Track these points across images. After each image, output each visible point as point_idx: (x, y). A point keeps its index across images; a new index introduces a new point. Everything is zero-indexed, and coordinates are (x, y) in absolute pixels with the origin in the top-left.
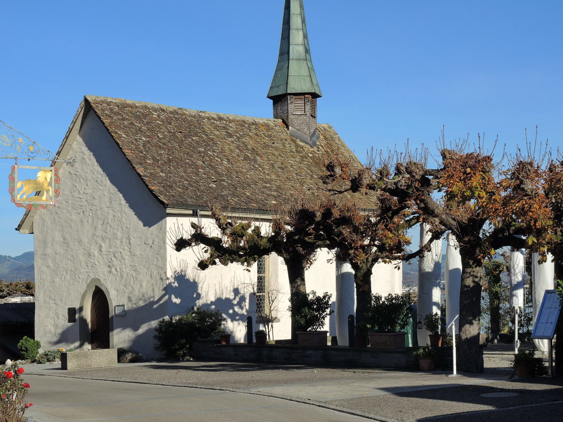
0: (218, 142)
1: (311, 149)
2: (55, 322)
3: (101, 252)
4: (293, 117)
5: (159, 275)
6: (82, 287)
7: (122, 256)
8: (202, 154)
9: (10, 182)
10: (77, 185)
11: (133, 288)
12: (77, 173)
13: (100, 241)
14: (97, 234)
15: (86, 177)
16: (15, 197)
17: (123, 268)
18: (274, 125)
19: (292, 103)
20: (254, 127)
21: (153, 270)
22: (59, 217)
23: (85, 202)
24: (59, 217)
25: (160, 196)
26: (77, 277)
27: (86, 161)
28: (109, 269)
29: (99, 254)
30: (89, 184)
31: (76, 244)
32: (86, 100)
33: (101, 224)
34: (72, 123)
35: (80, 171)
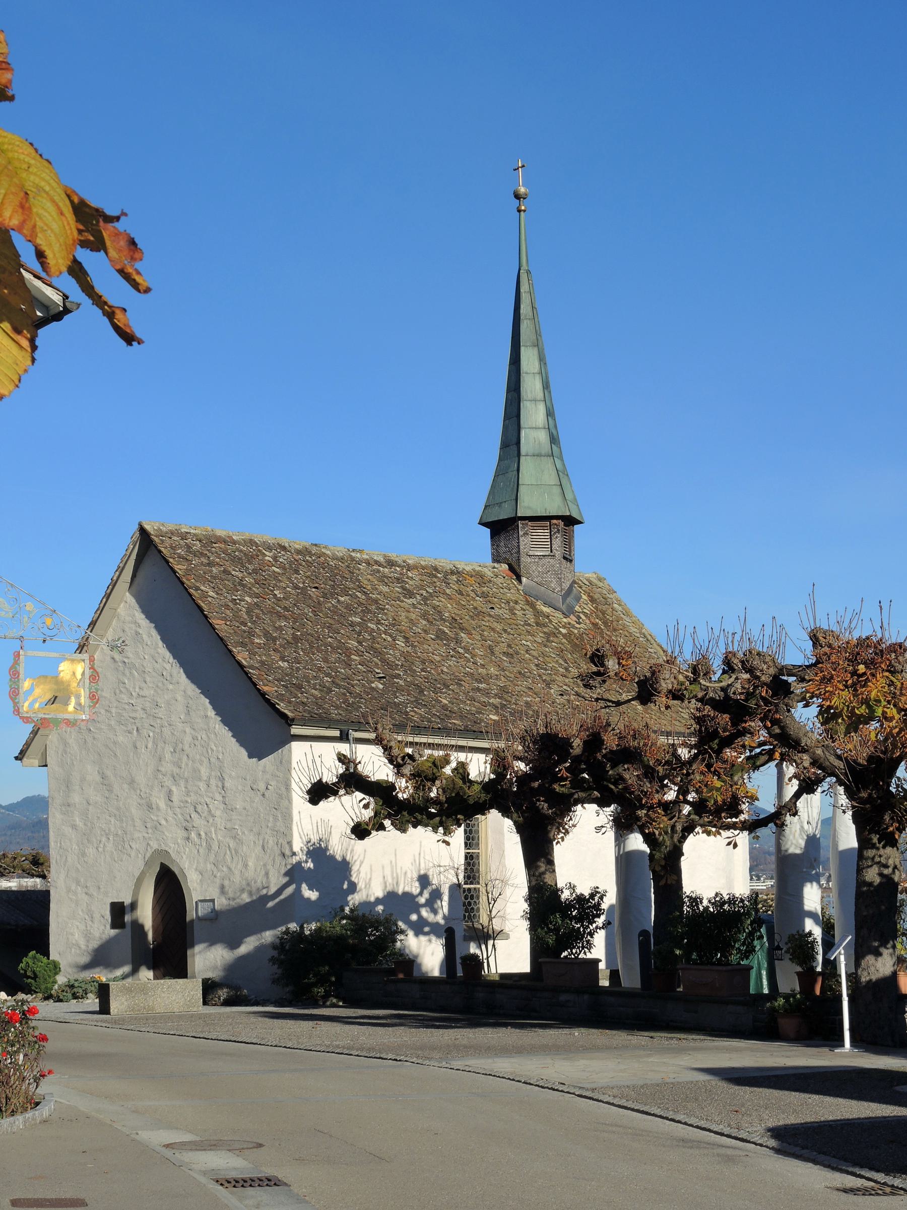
0: (387, 606)
1: (565, 620)
2: (86, 927)
3: (170, 803)
4: (529, 560)
5: (279, 846)
6: (136, 865)
7: (210, 811)
8: (358, 629)
9: (11, 680)
10: (126, 681)
11: (230, 869)
12: (126, 660)
13: (168, 782)
14: (163, 769)
15: (143, 666)
16: (20, 705)
17: (211, 832)
18: (492, 575)
19: (528, 534)
20: (454, 578)
21: (267, 837)
22: (94, 738)
23: (142, 712)
24: (94, 738)
25: (278, 704)
26: (127, 846)
27: (142, 638)
28: (185, 834)
29: (167, 805)
30: (148, 679)
31: (125, 786)
32: (142, 531)
33: (172, 752)
34: (117, 571)
35: (131, 656)
